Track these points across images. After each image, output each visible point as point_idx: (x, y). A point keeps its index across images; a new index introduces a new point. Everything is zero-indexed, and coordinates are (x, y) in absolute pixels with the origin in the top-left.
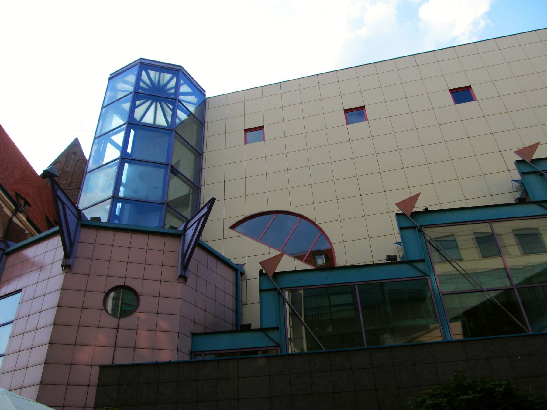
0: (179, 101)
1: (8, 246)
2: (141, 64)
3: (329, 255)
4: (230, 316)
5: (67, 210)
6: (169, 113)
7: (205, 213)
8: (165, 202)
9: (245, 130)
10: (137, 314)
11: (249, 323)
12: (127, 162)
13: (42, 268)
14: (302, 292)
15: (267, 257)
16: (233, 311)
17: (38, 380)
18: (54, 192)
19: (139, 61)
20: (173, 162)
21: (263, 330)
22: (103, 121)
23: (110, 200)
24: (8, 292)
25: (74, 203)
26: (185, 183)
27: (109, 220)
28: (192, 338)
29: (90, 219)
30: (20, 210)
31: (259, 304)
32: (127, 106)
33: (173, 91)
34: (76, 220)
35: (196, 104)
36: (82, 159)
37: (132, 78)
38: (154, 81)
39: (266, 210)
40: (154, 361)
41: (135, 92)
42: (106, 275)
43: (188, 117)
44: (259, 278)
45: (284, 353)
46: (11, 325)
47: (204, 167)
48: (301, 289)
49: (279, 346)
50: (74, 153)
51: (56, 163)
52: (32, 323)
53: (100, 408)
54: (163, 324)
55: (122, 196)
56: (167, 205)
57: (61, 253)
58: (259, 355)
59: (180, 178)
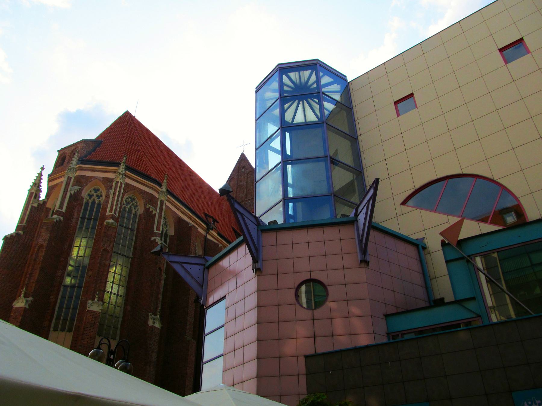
0: (323, 93)
1: (207, 261)
2: (280, 69)
3: (518, 210)
4: (420, 293)
5: (246, 219)
6: (316, 107)
7: (372, 195)
8: (332, 193)
9: (394, 102)
10: (328, 303)
11: (441, 297)
12: (289, 164)
13: (238, 275)
14: (495, 255)
15: (447, 226)
16: (423, 287)
17: (254, 374)
18: (232, 206)
19: (278, 67)
20: (331, 154)
21: (458, 302)
22: (260, 132)
23: (282, 202)
24: (215, 301)
25: (251, 210)
26: (347, 170)
27: (285, 221)
28: (386, 319)
29: (268, 224)
30: (211, 228)
31: (448, 277)
32: (277, 112)
33: (315, 85)
34: (256, 227)
35: (340, 90)
36: (251, 171)
37: (275, 85)
38: (295, 81)
39: (434, 178)
40: (353, 346)
41: (281, 97)
42: (293, 271)
43: (335, 107)
44: (443, 250)
45: (486, 323)
46: (224, 327)
47: (361, 150)
48: (494, 253)
49: (479, 316)
50: (244, 167)
51: (231, 179)
52: (239, 324)
53: (309, 394)
54: (355, 310)
55: (292, 196)
56: (335, 196)
57: (249, 259)
58: (462, 328)
59: (340, 167)
